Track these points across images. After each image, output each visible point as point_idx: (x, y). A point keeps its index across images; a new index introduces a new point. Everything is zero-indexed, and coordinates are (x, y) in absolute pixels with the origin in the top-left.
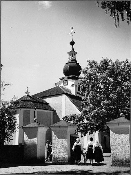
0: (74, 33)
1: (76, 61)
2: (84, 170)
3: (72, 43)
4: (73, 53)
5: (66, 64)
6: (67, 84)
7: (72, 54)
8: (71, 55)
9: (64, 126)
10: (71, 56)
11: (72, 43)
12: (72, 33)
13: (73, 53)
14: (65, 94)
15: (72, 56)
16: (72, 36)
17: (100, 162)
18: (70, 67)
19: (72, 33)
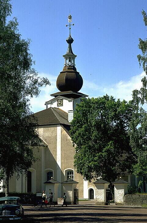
0: (73, 25)
1: (75, 69)
2: (33, 214)
3: (70, 41)
4: (71, 56)
5: (61, 73)
6: (62, 105)
7: (70, 58)
8: (68, 60)
9: (79, 209)
10: (68, 61)
11: (70, 41)
12: (70, 25)
13: (71, 56)
14: (61, 124)
15: (70, 61)
16: (70, 29)
17: (55, 206)
18: (67, 79)
19: (70, 25)
